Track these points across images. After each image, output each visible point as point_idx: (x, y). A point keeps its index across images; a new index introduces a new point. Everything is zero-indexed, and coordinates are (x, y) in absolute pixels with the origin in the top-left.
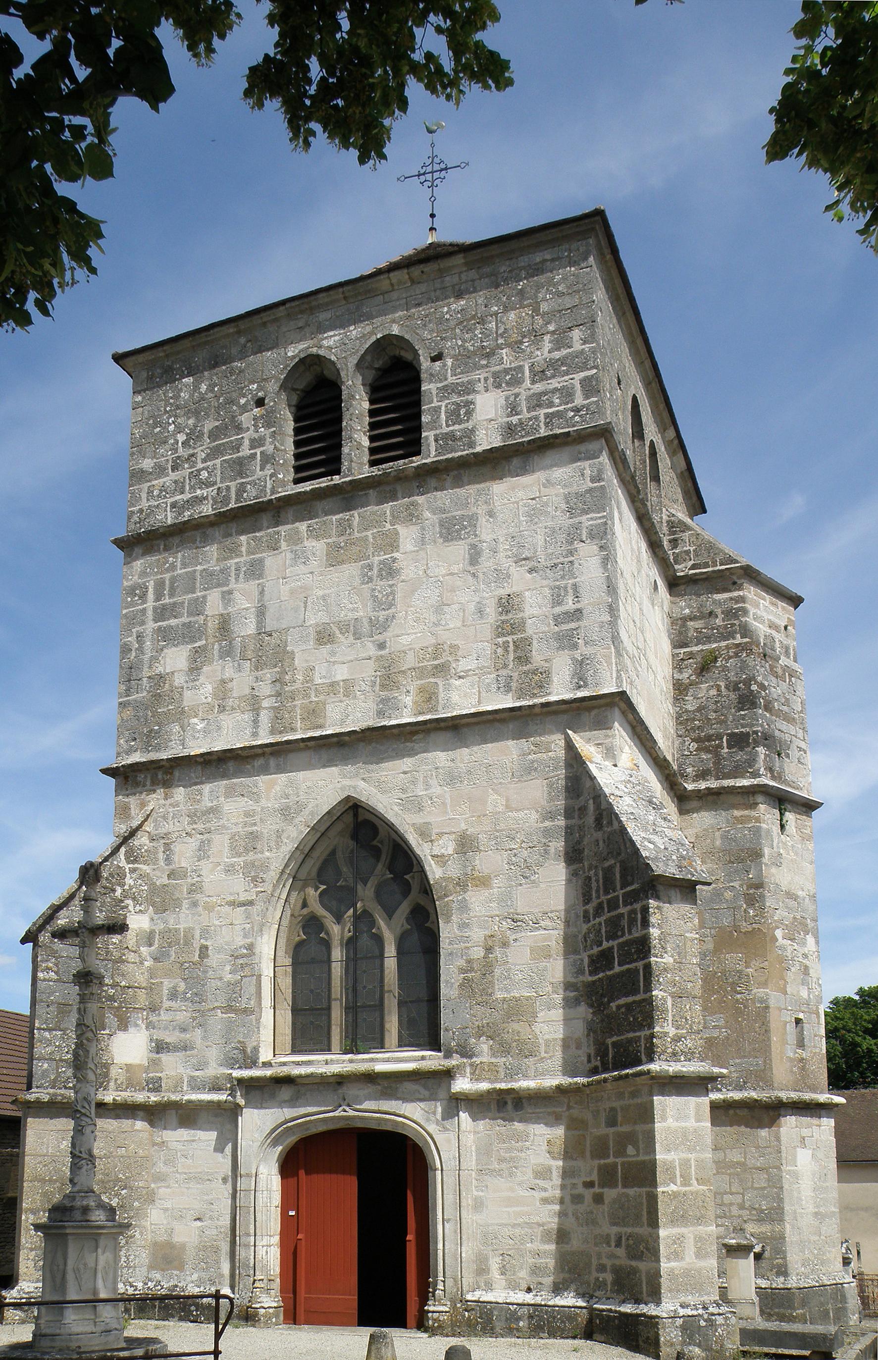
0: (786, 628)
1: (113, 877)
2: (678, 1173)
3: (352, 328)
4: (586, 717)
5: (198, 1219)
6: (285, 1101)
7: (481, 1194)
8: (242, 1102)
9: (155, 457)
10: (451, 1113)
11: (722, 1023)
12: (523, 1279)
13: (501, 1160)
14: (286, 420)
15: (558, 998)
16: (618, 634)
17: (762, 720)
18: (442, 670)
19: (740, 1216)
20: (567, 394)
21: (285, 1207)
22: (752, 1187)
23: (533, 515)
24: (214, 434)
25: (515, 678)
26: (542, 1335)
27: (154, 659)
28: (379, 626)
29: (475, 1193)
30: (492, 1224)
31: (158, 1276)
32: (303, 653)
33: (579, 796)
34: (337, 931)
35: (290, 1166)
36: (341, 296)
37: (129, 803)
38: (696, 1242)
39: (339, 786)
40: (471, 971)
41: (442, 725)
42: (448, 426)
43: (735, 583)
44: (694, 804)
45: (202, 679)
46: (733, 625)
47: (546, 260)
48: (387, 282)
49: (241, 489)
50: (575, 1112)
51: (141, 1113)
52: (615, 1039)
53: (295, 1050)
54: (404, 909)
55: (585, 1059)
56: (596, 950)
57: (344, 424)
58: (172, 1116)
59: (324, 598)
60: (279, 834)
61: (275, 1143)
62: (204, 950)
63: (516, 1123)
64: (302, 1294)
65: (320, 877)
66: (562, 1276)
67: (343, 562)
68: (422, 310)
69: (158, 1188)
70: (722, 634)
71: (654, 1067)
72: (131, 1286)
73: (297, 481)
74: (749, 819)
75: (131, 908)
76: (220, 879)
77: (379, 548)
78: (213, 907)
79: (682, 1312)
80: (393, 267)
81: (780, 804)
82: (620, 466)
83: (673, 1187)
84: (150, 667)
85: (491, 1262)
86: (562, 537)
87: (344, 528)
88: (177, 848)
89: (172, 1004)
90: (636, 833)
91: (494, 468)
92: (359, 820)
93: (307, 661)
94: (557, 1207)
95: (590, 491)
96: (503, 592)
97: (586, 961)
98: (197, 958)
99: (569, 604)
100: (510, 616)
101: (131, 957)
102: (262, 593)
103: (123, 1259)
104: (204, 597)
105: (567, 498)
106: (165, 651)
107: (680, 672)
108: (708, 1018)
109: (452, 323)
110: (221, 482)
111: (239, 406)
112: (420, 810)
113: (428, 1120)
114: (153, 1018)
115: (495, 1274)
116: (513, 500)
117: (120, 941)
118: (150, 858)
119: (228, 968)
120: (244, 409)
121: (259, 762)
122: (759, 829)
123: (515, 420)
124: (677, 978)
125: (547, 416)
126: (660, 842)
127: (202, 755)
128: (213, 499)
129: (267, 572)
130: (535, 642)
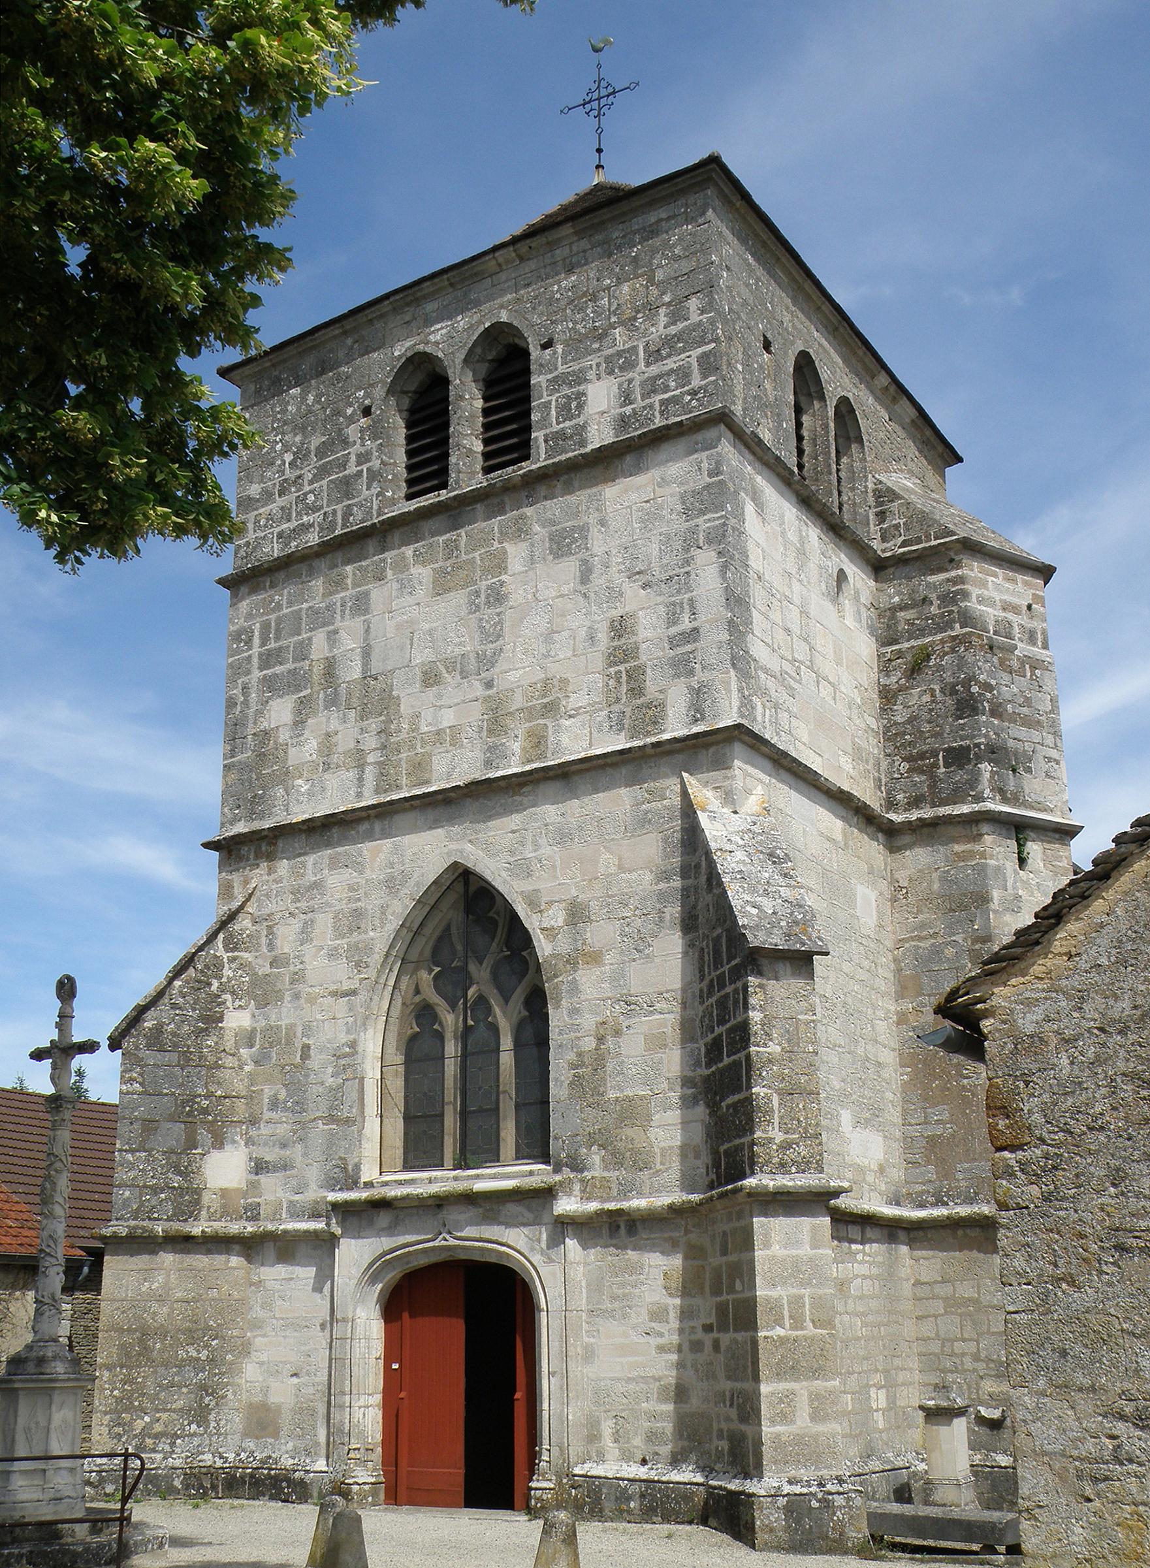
0: (1029, 607)
1: (209, 969)
2: (786, 1313)
3: (459, 318)
4: (705, 756)
5: (295, 1375)
6: (383, 1229)
7: (592, 1340)
8: (338, 1231)
9: (262, 481)
10: (556, 1241)
11: (946, 1116)
12: (637, 1447)
13: (614, 1298)
14: (395, 428)
15: (674, 1096)
16: (747, 652)
17: (986, 728)
18: (551, 709)
19: (975, 1370)
20: (683, 375)
21: (388, 1359)
22: (988, 1332)
23: (648, 519)
24: (321, 452)
25: (628, 715)
26: (655, 1519)
27: (259, 713)
28: (487, 661)
29: (586, 1339)
30: (604, 1378)
31: (251, 1444)
32: (410, 698)
33: (695, 851)
34: (450, 1020)
35: (394, 1307)
36: (446, 283)
37: (232, 880)
38: (811, 1401)
39: (446, 850)
40: (581, 1066)
41: (551, 773)
42: (558, 423)
43: (952, 561)
44: (907, 839)
45: (307, 733)
46: (951, 612)
47: (662, 220)
48: (494, 262)
49: (348, 513)
50: (693, 1237)
51: (237, 1247)
52: (726, 1146)
53: (407, 1166)
54: (519, 996)
55: (704, 1171)
56: (711, 1036)
57: (452, 429)
58: (270, 1250)
59: (430, 632)
60: (383, 909)
61: (373, 1280)
62: (306, 1048)
63: (629, 1252)
64: (404, 1461)
65: (436, 956)
66: (680, 1444)
67: (449, 590)
68: (530, 292)
69: (255, 1337)
70: (938, 624)
71: (750, 1182)
72: (221, 1457)
73: (409, 497)
74: (971, 855)
75: (229, 1004)
76: (324, 968)
77: (487, 572)
78: (316, 999)
79: (787, 1489)
80: (496, 249)
81: (1017, 833)
82: (757, 449)
83: (779, 1331)
84: (255, 723)
85: (602, 1427)
86: (678, 545)
87: (452, 549)
88: (280, 931)
89: (273, 1115)
90: (737, 896)
91: (606, 468)
92: (472, 889)
93: (412, 706)
94: (674, 1357)
95: (708, 486)
96: (615, 614)
97: (703, 1050)
98: (298, 1060)
99: (686, 624)
100: (623, 641)
101: (229, 1061)
102: (367, 631)
103: (213, 1424)
104: (310, 639)
105: (683, 498)
106: (271, 703)
107: (888, 676)
108: (929, 1110)
109: (563, 303)
110: (328, 506)
111: (345, 417)
112: (529, 875)
113: (532, 1249)
114: (253, 1132)
115: (608, 1442)
116: (626, 504)
117: (216, 1043)
118: (251, 943)
119: (330, 1070)
120: (351, 420)
121: (364, 827)
122: (984, 867)
123: (628, 410)
124: (786, 1071)
125: (662, 402)
126: (768, 905)
127: (304, 822)
128: (319, 525)
129: (373, 606)
130: (649, 671)
